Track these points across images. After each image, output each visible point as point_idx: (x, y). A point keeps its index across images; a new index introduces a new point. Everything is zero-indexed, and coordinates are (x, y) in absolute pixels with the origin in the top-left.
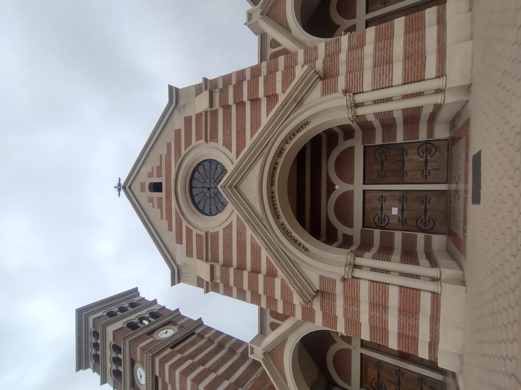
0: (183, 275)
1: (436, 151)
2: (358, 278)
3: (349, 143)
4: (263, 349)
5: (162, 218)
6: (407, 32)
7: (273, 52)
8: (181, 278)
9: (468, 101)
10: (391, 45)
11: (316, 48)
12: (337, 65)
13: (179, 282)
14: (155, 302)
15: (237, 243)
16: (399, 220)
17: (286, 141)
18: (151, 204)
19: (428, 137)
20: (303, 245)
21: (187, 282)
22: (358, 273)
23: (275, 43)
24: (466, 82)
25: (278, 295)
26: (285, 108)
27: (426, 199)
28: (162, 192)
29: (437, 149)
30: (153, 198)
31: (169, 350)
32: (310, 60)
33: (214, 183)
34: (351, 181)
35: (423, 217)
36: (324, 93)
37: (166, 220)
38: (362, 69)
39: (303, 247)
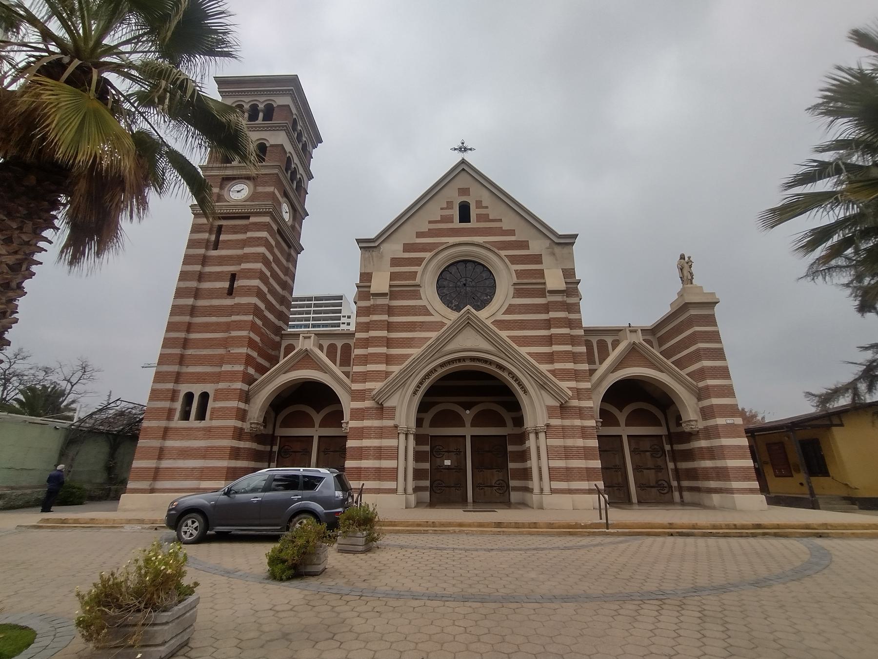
0: (369, 253)
1: (500, 493)
2: (398, 437)
3: (509, 422)
4: (311, 349)
5: (430, 222)
7: (608, 343)
8: (366, 251)
9: (533, 508)
10: (580, 458)
11: (590, 399)
12: (571, 418)
13: (361, 248)
14: (310, 177)
15: (412, 322)
16: (440, 466)
17: (510, 373)
18: (445, 206)
19: (512, 487)
20: (418, 390)
21: (363, 259)
22: (402, 437)
23: (615, 344)
24: (545, 506)
25: (371, 367)
26: (539, 375)
27: (459, 487)
28: (460, 222)
29: (502, 495)
30: (452, 208)
31: (275, 228)
32: (579, 394)
33: (472, 292)
34: (473, 425)
35: (444, 485)
36: (549, 409)
37: (429, 229)
38: (564, 437)
39: (417, 390)
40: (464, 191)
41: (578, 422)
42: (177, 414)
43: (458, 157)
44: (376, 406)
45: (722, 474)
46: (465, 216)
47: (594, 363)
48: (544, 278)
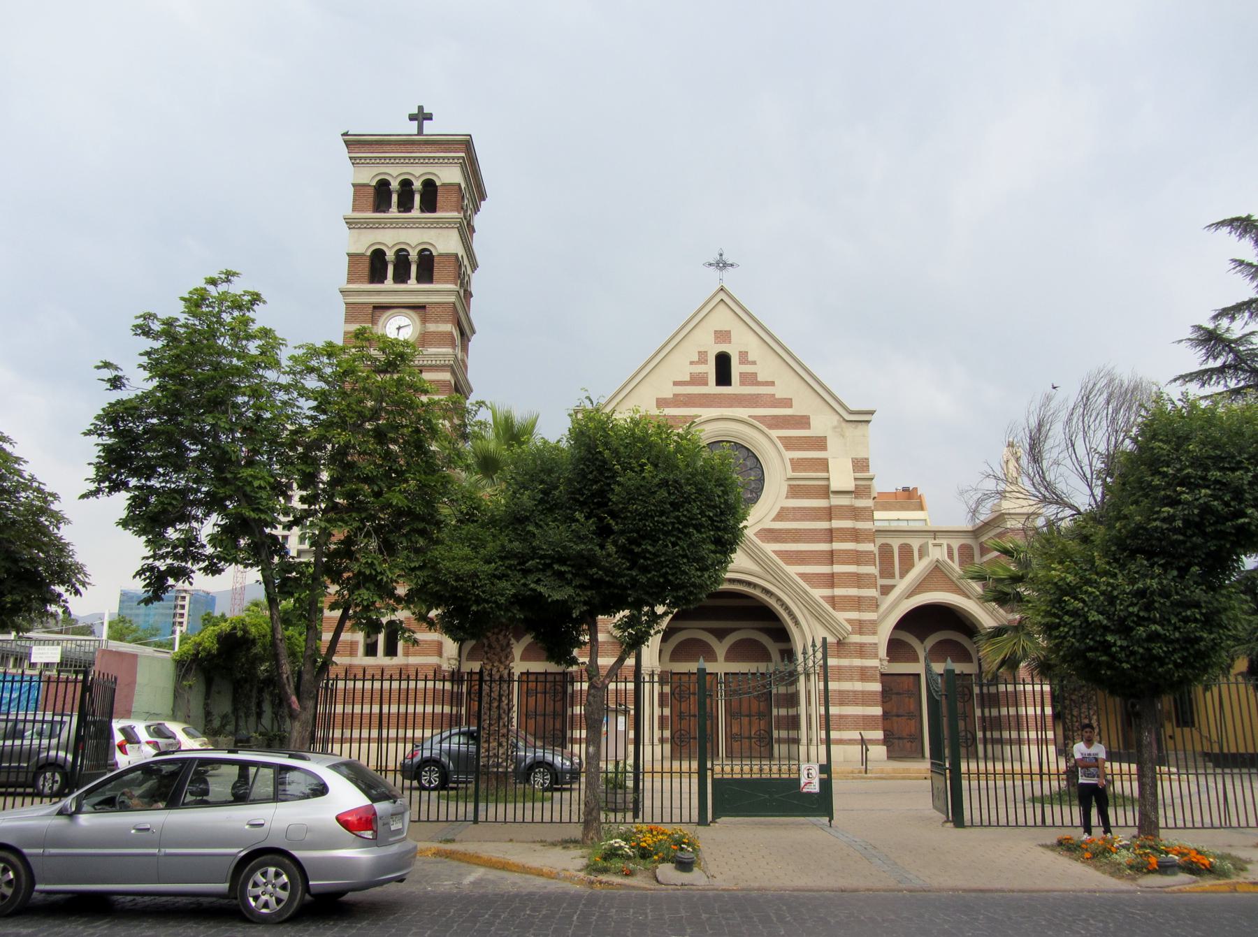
3: (775, 656)
5: (676, 383)
6: (451, 722)
10: (857, 704)
12: (850, 657)
17: (779, 600)
18: (696, 359)
32: (860, 627)
34: (729, 658)
37: (674, 395)
40: (722, 336)
41: (858, 662)
42: (361, 649)
43: (714, 278)
44: (611, 640)
45: (1018, 723)
46: (723, 376)
47: (892, 576)
48: (828, 471)
